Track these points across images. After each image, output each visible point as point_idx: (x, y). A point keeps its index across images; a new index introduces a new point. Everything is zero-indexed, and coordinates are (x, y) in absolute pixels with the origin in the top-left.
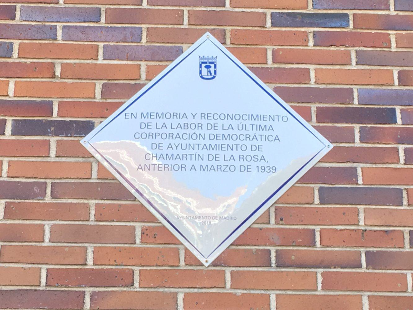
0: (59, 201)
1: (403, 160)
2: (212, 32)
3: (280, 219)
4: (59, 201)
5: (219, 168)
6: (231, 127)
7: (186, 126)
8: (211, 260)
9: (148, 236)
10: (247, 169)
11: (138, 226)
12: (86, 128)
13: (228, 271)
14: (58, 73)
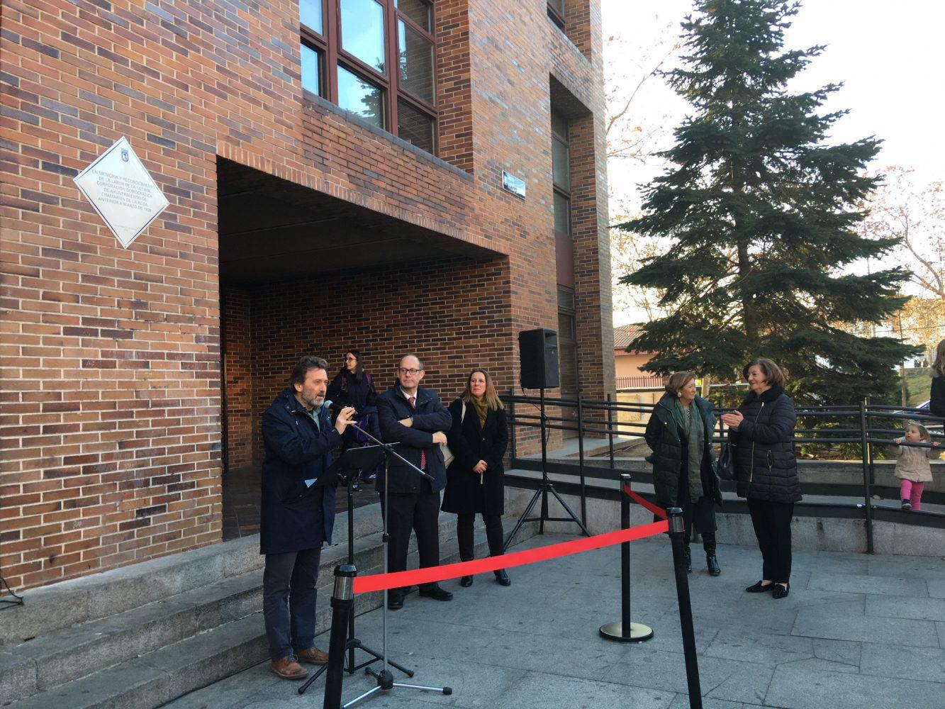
0: (65, 208)
1: (594, 112)
2: (125, 135)
3: (151, 233)
4: (65, 208)
5: (131, 205)
6: (134, 187)
7: (118, 183)
8: (127, 246)
9: (662, 130)
10: (141, 208)
11: (99, 227)
12: (75, 173)
13: (133, 252)
14: (60, 140)
